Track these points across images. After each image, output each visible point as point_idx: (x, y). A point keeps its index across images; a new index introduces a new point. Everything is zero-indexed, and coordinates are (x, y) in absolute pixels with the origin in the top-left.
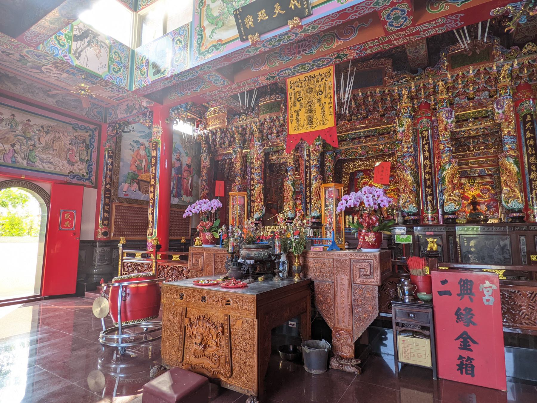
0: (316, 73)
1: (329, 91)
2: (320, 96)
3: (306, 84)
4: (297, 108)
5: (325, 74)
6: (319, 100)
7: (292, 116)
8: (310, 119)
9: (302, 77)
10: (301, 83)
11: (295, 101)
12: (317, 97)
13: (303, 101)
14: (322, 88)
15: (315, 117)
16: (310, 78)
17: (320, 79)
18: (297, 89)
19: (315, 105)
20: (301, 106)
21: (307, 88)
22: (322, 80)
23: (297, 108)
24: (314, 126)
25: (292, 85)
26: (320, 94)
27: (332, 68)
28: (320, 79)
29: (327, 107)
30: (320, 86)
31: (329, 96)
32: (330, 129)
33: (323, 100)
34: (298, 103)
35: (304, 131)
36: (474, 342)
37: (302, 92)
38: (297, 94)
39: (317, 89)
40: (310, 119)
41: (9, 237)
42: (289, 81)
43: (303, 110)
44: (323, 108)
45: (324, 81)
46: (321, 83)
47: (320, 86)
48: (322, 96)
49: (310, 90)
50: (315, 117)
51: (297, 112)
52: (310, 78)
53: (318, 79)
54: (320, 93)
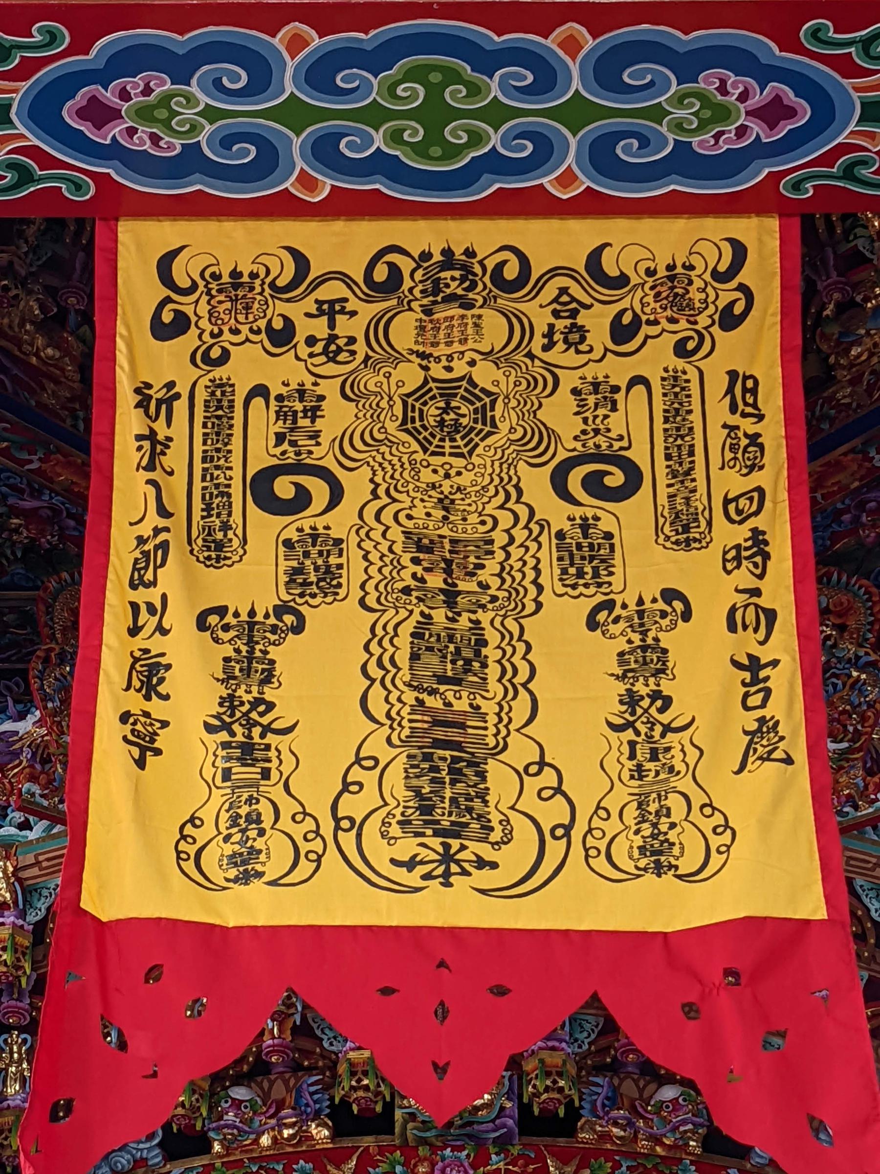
0: (555, 243)
1: (734, 482)
2: (607, 516)
3: (404, 331)
4: (254, 580)
5: (673, 287)
6: (588, 557)
7: (149, 675)
8: (449, 779)
9: (343, 246)
10: (330, 310)
11: (216, 499)
12: (557, 514)
13: (340, 523)
14: (635, 425)
15: (521, 751)
16: (454, 281)
17: (597, 323)
18: (249, 365)
19: (520, 603)
20: (313, 573)
21: (410, 375)
22: (622, 332)
23: (254, 580)
24: (514, 860)
25: (195, 307)
26: (594, 485)
27: (762, 235)
28: (597, 323)
29: (700, 666)
30: (606, 394)
31: (728, 535)
32: (765, 942)
33: (644, 565)
34: (265, 530)
35: (336, 900)
36: (163, 655)
37: (337, 417)
38: (262, 421)
39: (560, 415)
40: (449, 779)
41: (409, 650)
42: (137, 246)
43: (337, 630)
44: (647, 660)
45: (656, 357)
46: (618, 370)
47: (606, 394)
48: (632, 521)
49: (448, 416)
50: (521, 751)
51: (249, 649)
52: (454, 281)
53: (567, 307)
54: (609, 474)
